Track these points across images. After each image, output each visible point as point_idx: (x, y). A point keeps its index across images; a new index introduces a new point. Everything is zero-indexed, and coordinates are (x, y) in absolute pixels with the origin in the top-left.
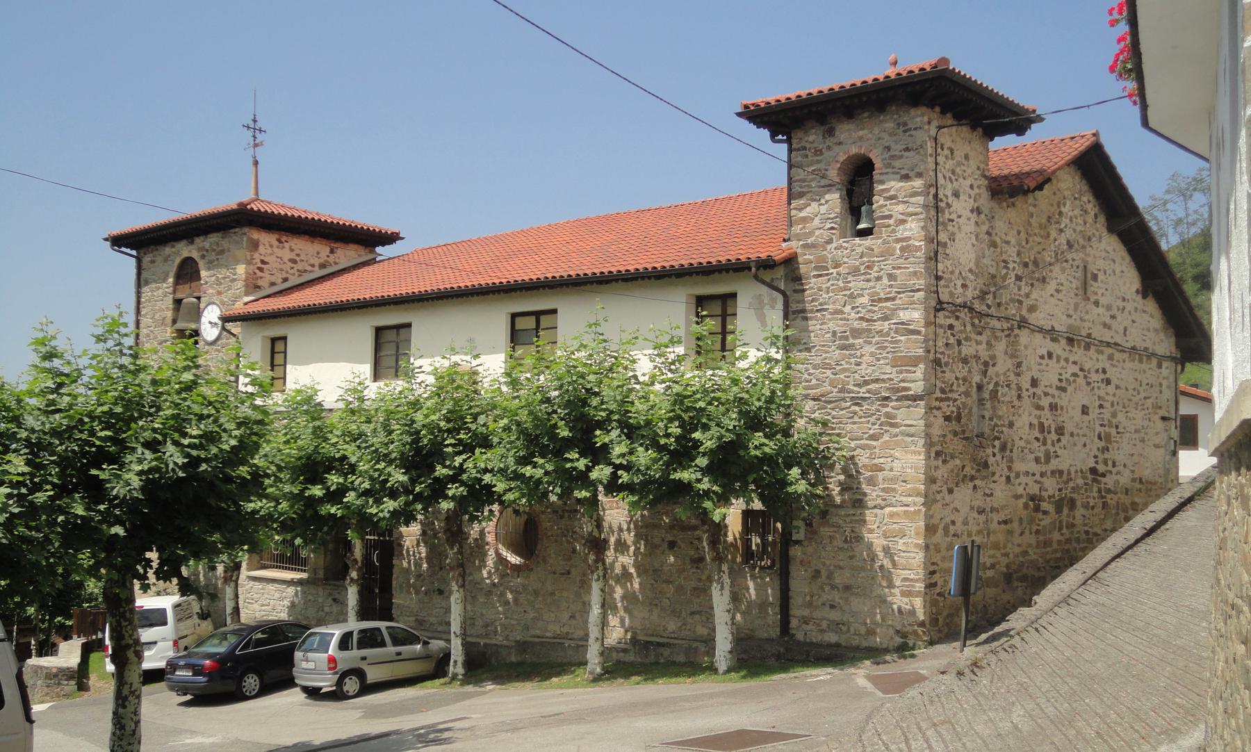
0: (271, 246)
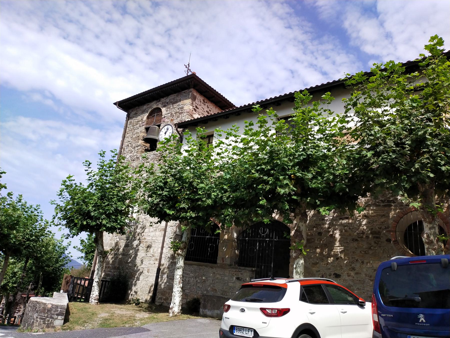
0: (201, 102)
